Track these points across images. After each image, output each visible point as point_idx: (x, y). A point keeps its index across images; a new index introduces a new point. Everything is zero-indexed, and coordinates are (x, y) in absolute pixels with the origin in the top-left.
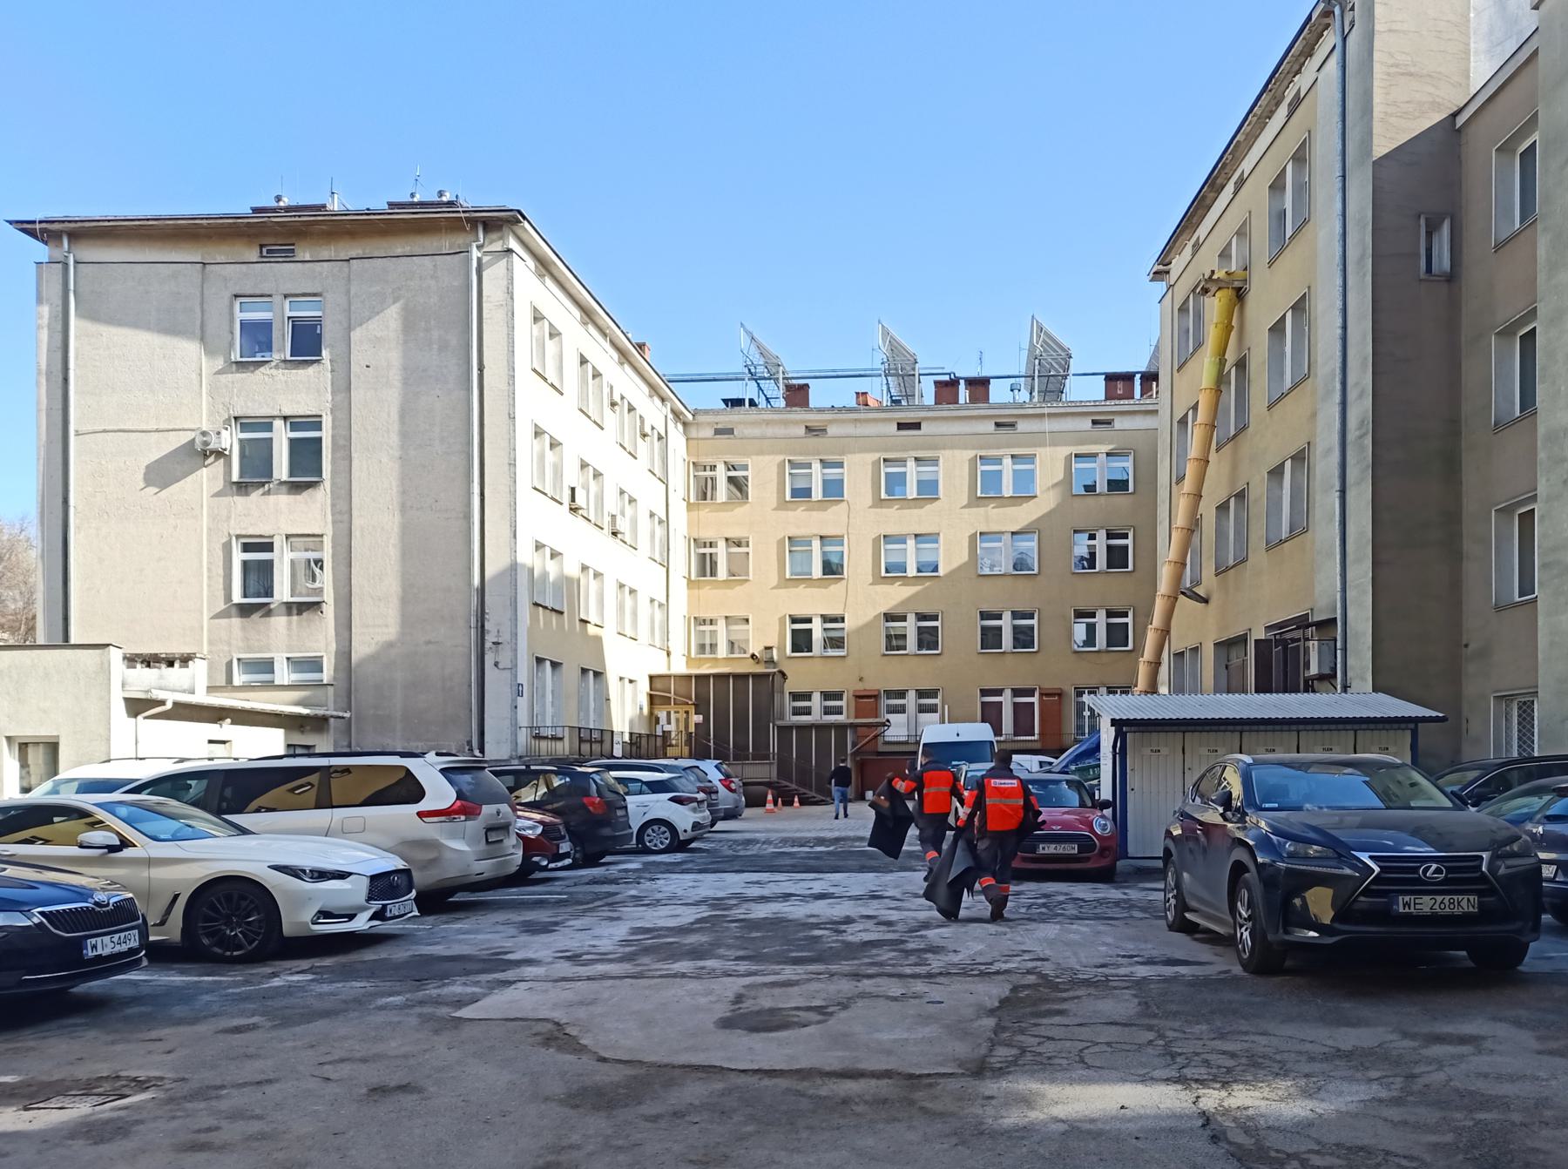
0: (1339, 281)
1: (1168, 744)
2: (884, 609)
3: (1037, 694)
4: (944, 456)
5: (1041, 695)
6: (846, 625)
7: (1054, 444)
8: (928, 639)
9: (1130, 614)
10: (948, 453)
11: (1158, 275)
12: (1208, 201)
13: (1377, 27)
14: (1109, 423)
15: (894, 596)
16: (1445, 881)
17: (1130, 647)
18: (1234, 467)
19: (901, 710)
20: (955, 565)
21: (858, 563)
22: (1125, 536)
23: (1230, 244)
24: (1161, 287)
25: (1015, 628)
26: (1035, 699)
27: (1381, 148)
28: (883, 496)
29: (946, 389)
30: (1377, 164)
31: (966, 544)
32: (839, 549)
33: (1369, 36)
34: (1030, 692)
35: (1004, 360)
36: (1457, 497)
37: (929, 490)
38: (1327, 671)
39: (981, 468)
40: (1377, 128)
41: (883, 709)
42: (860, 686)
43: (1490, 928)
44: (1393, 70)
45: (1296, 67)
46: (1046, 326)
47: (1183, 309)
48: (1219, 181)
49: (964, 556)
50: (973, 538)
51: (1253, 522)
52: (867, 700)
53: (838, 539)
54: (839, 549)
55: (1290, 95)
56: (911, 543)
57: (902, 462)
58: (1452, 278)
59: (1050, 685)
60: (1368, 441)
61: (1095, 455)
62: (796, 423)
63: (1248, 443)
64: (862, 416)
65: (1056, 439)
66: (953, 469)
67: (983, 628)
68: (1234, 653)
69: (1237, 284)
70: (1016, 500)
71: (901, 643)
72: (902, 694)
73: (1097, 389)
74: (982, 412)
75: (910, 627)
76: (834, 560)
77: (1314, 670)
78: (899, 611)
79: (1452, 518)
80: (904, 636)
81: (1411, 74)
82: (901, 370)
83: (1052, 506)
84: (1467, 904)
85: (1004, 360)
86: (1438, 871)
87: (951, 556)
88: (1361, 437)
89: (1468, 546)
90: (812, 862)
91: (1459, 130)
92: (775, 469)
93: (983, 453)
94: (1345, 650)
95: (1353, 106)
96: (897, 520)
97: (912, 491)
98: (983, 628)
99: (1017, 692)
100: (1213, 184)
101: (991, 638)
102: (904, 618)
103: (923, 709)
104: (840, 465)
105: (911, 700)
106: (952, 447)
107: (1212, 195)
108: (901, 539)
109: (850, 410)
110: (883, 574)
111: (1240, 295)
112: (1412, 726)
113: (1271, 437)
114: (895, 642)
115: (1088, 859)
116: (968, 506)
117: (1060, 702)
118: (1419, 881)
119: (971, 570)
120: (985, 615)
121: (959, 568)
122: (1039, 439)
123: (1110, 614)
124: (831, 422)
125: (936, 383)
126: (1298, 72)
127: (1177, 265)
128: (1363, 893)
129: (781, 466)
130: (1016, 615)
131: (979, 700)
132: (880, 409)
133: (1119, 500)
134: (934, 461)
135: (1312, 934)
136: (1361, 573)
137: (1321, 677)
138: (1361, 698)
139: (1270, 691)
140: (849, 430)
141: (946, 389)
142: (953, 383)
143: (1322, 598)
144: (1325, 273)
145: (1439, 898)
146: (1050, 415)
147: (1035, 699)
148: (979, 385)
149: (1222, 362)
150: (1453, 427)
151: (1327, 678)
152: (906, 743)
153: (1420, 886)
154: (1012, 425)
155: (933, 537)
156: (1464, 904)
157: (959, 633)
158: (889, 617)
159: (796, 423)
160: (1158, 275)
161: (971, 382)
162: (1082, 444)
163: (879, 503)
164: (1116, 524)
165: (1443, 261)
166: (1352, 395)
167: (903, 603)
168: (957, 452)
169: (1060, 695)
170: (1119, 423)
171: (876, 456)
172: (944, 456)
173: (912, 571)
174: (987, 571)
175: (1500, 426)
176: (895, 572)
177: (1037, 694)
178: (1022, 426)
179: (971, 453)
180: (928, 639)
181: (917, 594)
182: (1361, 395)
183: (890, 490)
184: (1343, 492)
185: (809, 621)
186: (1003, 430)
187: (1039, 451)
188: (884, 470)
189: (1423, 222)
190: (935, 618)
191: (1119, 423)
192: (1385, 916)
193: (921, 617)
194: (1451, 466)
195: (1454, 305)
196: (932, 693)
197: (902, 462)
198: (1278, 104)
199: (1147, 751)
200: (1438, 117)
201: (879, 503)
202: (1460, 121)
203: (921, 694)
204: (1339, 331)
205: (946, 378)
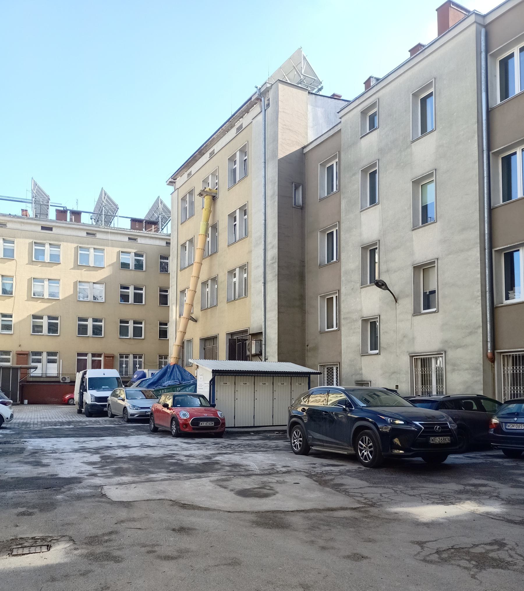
0: (263, 202)
1: (230, 379)
2: (33, 313)
3: (103, 356)
4: (63, 245)
5: (105, 357)
6: (13, 319)
7: (112, 246)
8: (53, 328)
9: (143, 323)
10: (65, 244)
11: (172, 183)
12: (197, 158)
13: (280, 110)
14: (135, 240)
15: (38, 307)
16: (442, 432)
17: (143, 337)
18: (211, 267)
19: (39, 361)
20: (67, 295)
21: (20, 289)
22: (142, 289)
23: (208, 177)
24: (171, 189)
25: (94, 326)
26: (102, 359)
27: (281, 155)
28: (34, 259)
29: (62, 214)
30: (280, 161)
31: (72, 286)
32: (11, 282)
33: (277, 112)
34: (100, 355)
35: (87, 204)
36: (304, 289)
37: (55, 261)
38: (258, 353)
39: (34, 247)
40: (280, 148)
41: (30, 361)
42: (19, 349)
43: (450, 448)
44: (284, 127)
45: (241, 115)
46: (38, 183)
47: (183, 199)
48: (203, 151)
49: (71, 292)
50: (75, 284)
51: (220, 292)
52: (22, 356)
53: (11, 278)
54: (11, 282)
55: (237, 125)
56: (46, 283)
57: (43, 245)
58: (302, 208)
59: (109, 352)
60: (276, 265)
61: (129, 253)
62: (38, 224)
63: (217, 258)
64: (25, 221)
65: (113, 244)
66: (67, 251)
67: (79, 325)
68: (208, 343)
69: (213, 195)
70: (96, 268)
71: (39, 329)
72: (40, 353)
73: (127, 224)
74: (64, 225)
75: (45, 323)
76: (8, 288)
77: (253, 352)
78: (40, 314)
79: (302, 297)
80: (42, 326)
81: (290, 130)
82: (41, 202)
83: (109, 274)
84: (447, 440)
85: (87, 204)
86: (439, 428)
87: (65, 291)
88: (272, 263)
89: (307, 308)
90: (101, 433)
91: (304, 154)
92: (27, 246)
93: (81, 246)
94: (265, 345)
95: (270, 138)
96: (38, 271)
97: (47, 259)
98: (79, 325)
99: (93, 355)
100: (201, 152)
101: (82, 330)
102: (41, 318)
103: (50, 361)
104: (13, 242)
105: (44, 357)
106: (67, 242)
107: (199, 156)
108: (42, 280)
109: (18, 217)
110: (32, 296)
111: (214, 198)
112: (308, 375)
113: (229, 257)
114: (37, 329)
115: (217, 428)
116: (74, 268)
117: (113, 360)
118: (434, 432)
119: (76, 299)
120: (80, 319)
121: (69, 297)
122: (106, 243)
123: (135, 323)
124: (9, 221)
125: (57, 210)
126: (242, 117)
127: (180, 181)
128: (420, 437)
129: (31, 244)
130: (95, 320)
131: (77, 358)
132: (32, 219)
133: (139, 274)
134: (58, 246)
135: (401, 452)
136: (273, 315)
137: (256, 355)
138: (272, 363)
139: (235, 359)
140: (18, 226)
141: (62, 214)
142: (64, 212)
143: (254, 323)
144: (258, 197)
145: (441, 438)
146: (111, 233)
147: (102, 359)
148: (77, 214)
149: (207, 224)
150: (303, 264)
151: (259, 355)
152: (41, 377)
153: (437, 434)
154: (94, 234)
155: (57, 281)
156: (447, 439)
157: (68, 327)
158: (35, 317)
159: (38, 224)
160: (172, 183)
161: (73, 213)
162: (124, 248)
163: (31, 262)
164: (138, 284)
165: (300, 201)
166: (269, 247)
167: (42, 310)
168: (69, 244)
169: (113, 357)
170: (99, 236)
171: (31, 241)
172: (63, 245)
173: (46, 296)
174: (81, 299)
175: (321, 266)
176: (36, 297)
177: (103, 356)
178: (99, 236)
179: (76, 245)
180: (53, 328)
181: (49, 307)
182: (273, 247)
183: (36, 258)
184: (265, 283)
185: (127, 322)
186: (89, 236)
187: (106, 248)
188: (34, 247)
189: (294, 185)
190: (56, 319)
191: (140, 240)
192: (427, 444)
193: (50, 318)
194: (302, 277)
195: (303, 218)
196: (54, 354)
197: (43, 245)
198: (232, 127)
199: (297, 384)
200: (298, 148)
201: (31, 262)
202: (306, 150)
203: (49, 354)
204: (264, 221)
205: (62, 209)
